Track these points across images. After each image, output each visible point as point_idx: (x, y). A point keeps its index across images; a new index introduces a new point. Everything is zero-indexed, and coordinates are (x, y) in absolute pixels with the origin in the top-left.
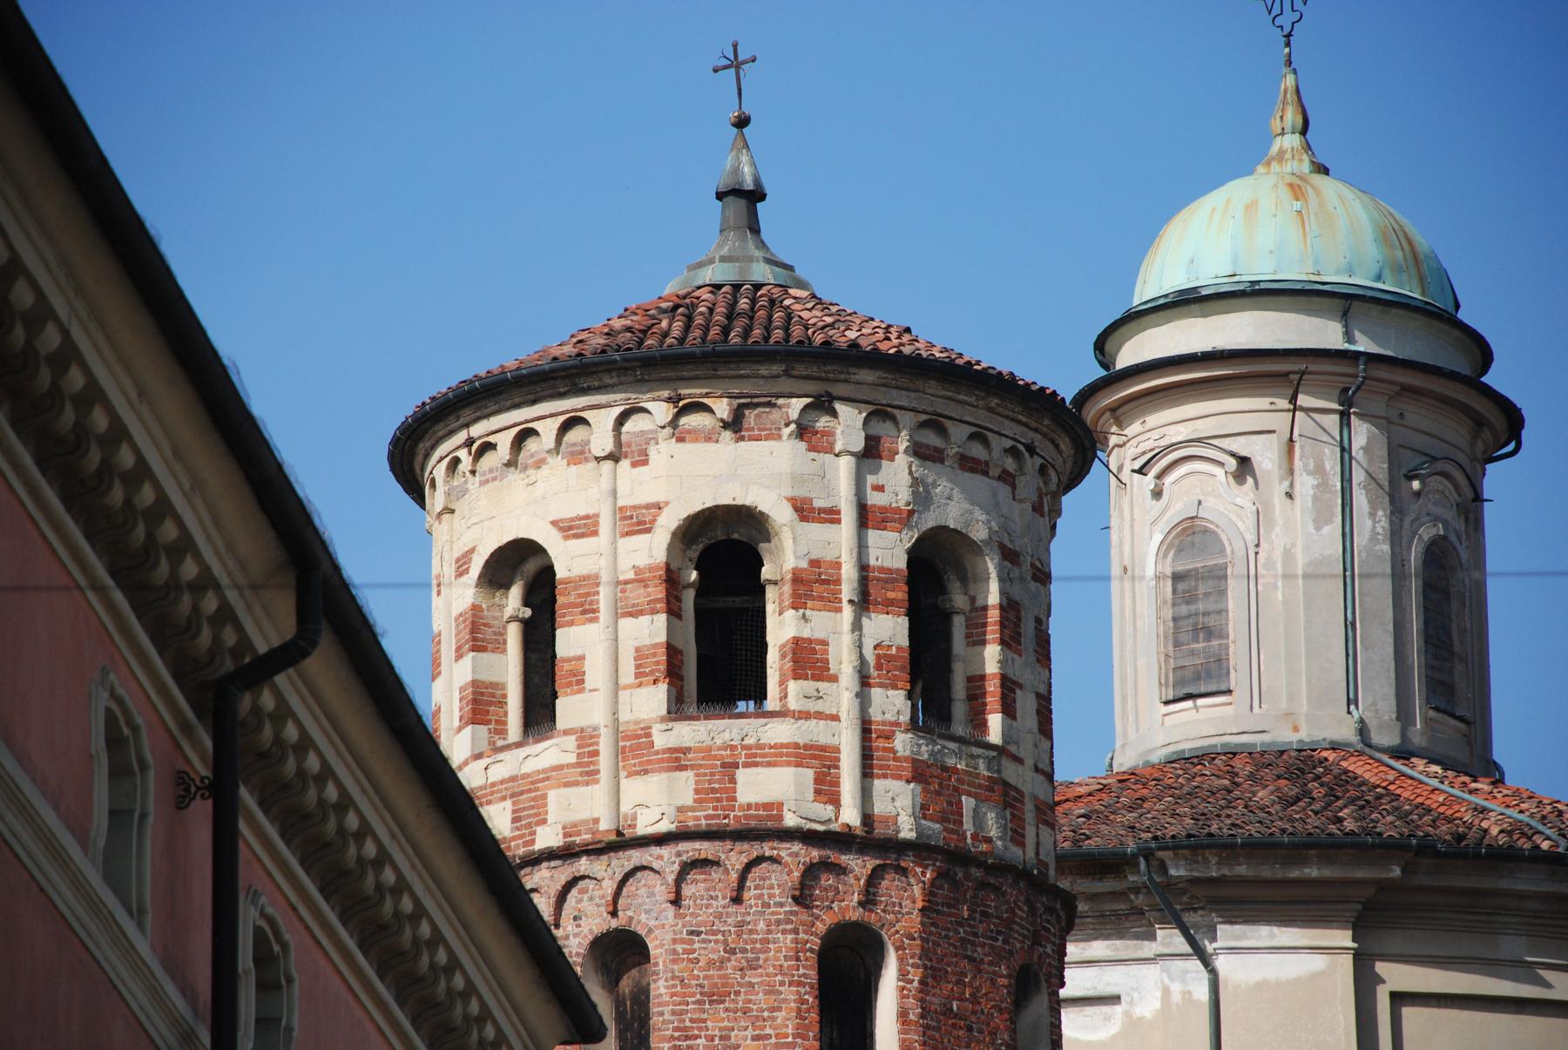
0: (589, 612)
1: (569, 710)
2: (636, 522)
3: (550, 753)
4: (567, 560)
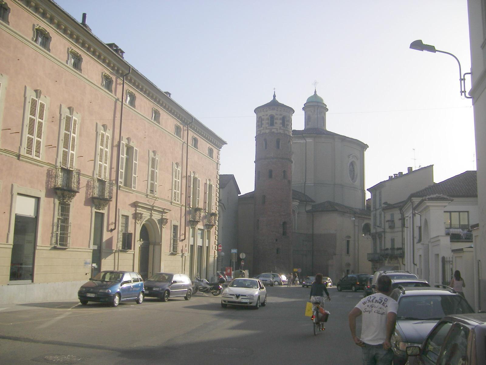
0: (264, 120)
1: (263, 126)
2: (267, 115)
3: (262, 128)
4: (263, 117)
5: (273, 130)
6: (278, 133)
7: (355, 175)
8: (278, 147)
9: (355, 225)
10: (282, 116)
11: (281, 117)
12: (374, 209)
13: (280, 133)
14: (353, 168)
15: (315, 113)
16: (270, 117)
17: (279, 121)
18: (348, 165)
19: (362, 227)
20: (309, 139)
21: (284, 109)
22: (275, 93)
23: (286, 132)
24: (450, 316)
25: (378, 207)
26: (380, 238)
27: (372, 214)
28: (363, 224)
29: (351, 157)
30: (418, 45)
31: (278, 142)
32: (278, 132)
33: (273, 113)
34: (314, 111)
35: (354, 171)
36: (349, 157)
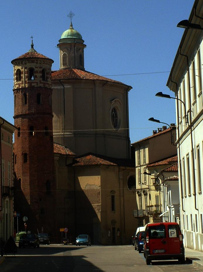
3: (20, 82)
5: (33, 84)
6: (38, 87)
7: (118, 121)
8: (38, 102)
9: (119, 178)
10: (42, 69)
11: (41, 70)
12: (138, 164)
13: (40, 87)
14: (116, 114)
15: (72, 51)
16: (30, 71)
17: (39, 75)
18: (111, 111)
19: (128, 179)
20: (66, 85)
21: (44, 62)
22: (32, 43)
23: (47, 86)
24: (137, 233)
25: (142, 163)
26: (146, 195)
27: (137, 169)
28: (128, 177)
29: (114, 102)
30: (152, 119)
31: (38, 96)
32: (39, 86)
33: (33, 65)
34: (71, 49)
35: (116, 117)
36: (111, 103)
